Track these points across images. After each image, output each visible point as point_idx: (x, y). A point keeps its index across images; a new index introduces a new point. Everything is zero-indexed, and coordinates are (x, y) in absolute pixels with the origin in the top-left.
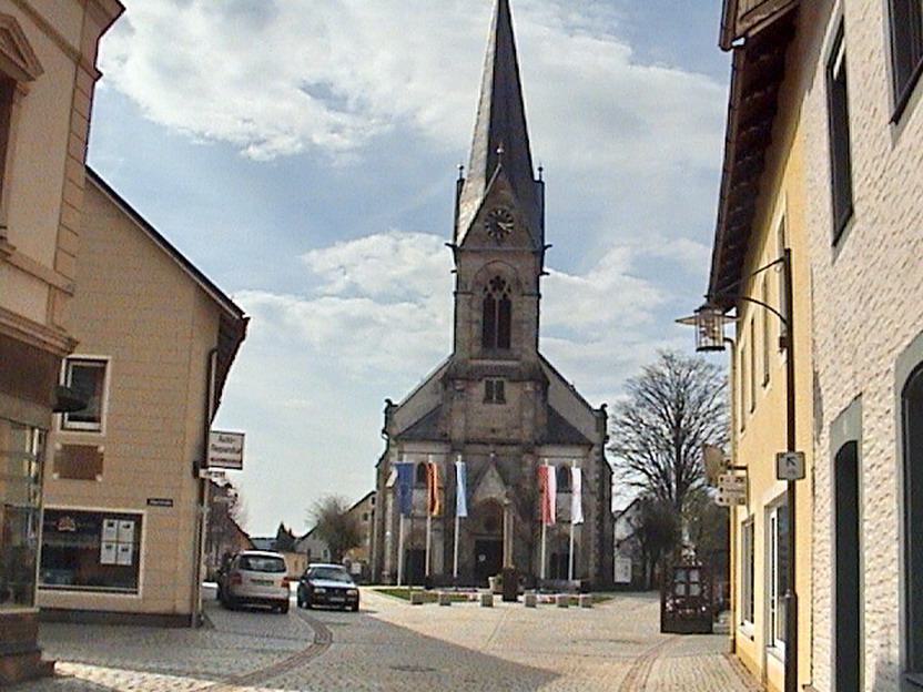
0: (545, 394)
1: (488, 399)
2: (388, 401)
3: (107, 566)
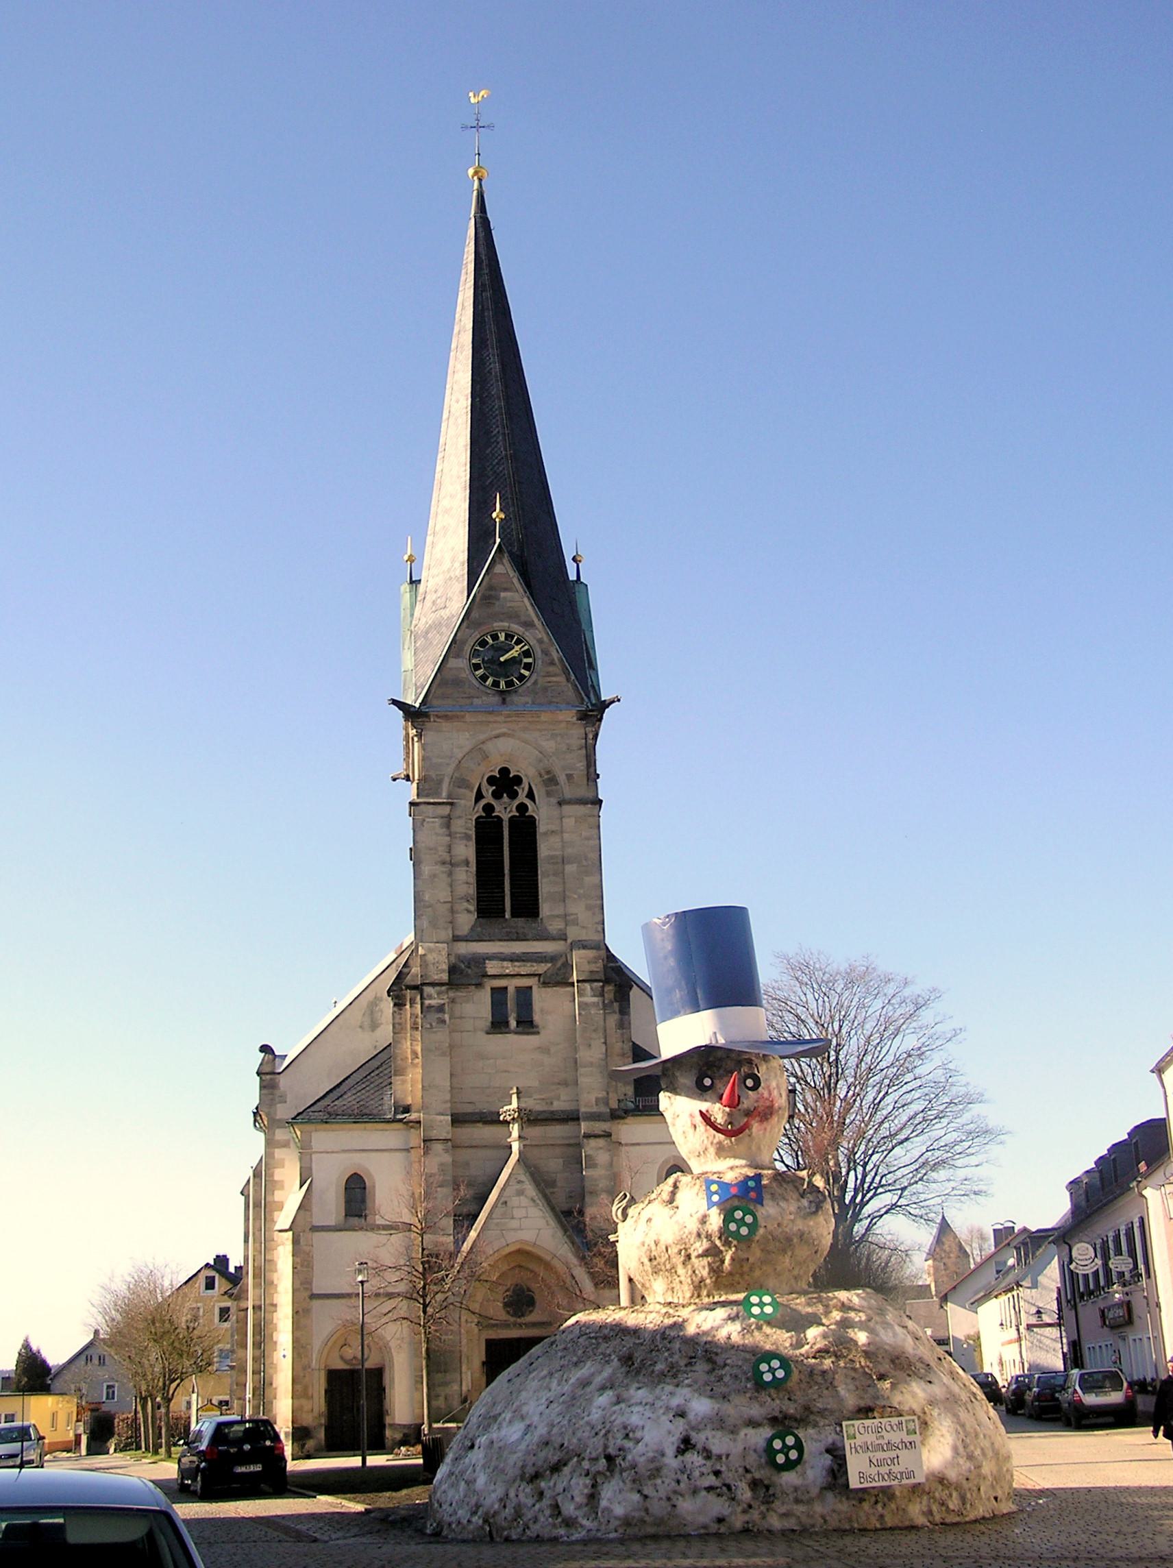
0: (624, 1010)
1: (498, 1025)
2: (265, 1049)
3: (424, 1461)
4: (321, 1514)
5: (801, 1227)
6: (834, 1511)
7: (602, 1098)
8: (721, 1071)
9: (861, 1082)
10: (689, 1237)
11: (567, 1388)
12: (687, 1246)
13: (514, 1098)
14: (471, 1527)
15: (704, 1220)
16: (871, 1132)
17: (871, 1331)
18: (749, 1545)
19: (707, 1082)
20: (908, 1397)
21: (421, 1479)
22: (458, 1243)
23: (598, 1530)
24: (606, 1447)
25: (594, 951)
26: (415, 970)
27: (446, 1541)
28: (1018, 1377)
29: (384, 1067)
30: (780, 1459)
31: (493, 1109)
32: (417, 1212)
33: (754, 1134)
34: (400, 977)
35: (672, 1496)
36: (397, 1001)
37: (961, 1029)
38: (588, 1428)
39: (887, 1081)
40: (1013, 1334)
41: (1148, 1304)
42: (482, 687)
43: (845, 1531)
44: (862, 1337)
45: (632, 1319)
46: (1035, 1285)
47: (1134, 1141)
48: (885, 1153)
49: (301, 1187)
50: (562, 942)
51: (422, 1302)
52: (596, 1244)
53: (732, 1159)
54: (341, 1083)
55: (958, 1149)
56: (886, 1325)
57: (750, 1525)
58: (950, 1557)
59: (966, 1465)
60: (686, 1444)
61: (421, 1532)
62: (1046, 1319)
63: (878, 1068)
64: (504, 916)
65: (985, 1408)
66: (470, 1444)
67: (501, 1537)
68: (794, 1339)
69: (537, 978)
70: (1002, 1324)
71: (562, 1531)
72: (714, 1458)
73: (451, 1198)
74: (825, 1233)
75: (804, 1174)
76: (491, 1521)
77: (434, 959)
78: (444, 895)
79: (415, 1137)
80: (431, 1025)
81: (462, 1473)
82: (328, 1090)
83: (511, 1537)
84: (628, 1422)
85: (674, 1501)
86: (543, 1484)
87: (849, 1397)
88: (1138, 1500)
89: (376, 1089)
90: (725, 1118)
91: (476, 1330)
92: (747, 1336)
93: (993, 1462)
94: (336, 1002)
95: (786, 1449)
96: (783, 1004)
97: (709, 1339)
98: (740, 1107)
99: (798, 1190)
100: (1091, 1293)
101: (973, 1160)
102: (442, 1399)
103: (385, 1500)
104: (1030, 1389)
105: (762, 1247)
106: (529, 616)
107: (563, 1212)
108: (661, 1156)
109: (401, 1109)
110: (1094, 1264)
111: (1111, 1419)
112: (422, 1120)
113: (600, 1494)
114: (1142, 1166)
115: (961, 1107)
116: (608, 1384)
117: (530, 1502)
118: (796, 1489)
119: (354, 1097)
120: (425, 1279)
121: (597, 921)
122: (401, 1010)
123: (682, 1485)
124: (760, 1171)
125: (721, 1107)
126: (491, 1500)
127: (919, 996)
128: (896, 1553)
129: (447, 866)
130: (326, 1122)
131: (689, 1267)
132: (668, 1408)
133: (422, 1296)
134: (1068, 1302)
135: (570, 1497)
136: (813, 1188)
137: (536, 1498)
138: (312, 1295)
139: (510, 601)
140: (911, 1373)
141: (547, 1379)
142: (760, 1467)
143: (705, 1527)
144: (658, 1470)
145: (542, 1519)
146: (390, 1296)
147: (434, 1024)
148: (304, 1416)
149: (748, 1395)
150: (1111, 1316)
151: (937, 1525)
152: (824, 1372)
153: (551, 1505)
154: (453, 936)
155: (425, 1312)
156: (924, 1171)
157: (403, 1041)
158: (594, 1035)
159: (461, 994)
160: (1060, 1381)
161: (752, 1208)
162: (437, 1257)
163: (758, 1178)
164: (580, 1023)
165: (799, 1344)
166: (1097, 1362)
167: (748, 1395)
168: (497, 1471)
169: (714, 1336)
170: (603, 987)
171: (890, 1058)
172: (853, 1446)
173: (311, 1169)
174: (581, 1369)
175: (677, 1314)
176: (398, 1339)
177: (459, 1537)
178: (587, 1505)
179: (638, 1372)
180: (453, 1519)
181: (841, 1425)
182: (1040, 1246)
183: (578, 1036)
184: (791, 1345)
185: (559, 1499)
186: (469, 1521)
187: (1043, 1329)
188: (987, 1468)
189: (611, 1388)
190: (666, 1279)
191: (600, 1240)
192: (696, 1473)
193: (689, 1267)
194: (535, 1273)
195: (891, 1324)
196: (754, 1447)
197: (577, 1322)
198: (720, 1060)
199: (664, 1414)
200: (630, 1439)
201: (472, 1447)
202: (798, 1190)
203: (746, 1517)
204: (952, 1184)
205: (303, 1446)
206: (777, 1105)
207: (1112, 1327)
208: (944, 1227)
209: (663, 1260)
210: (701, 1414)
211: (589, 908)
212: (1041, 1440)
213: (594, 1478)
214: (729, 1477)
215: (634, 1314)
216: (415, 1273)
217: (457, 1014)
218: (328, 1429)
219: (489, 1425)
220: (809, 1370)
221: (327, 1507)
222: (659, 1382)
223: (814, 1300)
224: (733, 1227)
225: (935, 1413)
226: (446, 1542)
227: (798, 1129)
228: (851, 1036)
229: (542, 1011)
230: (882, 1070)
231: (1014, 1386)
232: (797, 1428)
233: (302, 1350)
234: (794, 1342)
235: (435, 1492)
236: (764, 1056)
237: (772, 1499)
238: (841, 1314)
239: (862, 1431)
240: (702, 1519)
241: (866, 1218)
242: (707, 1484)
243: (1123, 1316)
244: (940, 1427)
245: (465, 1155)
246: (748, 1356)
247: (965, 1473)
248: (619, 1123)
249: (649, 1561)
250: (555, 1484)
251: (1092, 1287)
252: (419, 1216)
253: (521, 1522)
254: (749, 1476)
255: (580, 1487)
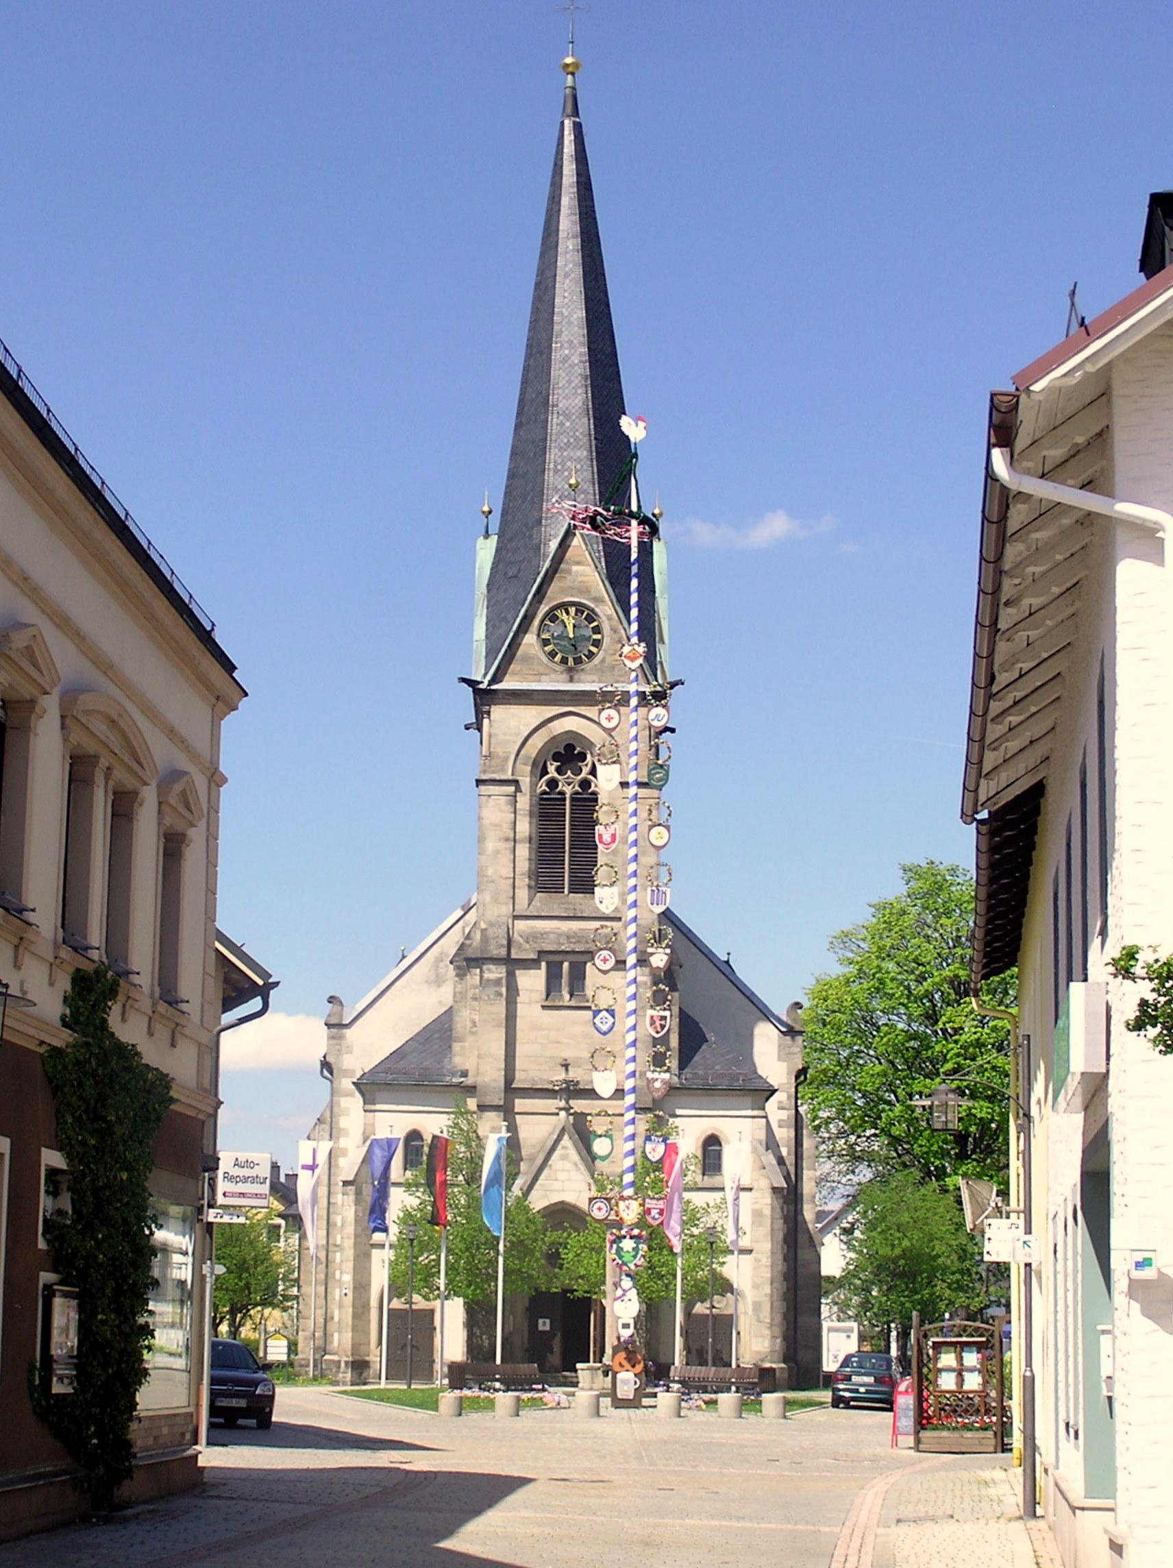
42: (550, 664)
49: (364, 1143)
106: (599, 591)
139: (582, 575)
147: (492, 997)
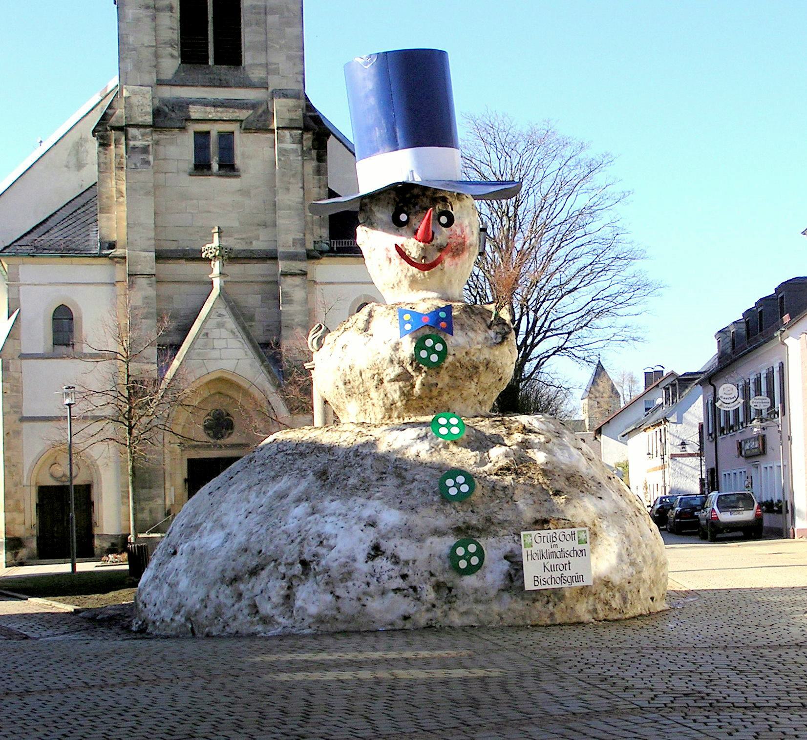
0: (321, 158)
1: (201, 167)
4: (32, 614)
5: (487, 357)
6: (509, 610)
7: (299, 240)
8: (417, 208)
9: (537, 235)
10: (382, 363)
11: (264, 500)
12: (380, 371)
13: (216, 236)
14: (174, 625)
15: (396, 348)
16: (543, 281)
17: (549, 452)
18: (433, 639)
19: (403, 217)
20: (580, 511)
21: (127, 582)
22: (162, 371)
23: (293, 627)
24: (301, 553)
25: (294, 100)
26: (120, 111)
27: (150, 636)
28: (662, 498)
29: (91, 204)
30: (463, 564)
31: (196, 247)
32: (122, 342)
33: (445, 269)
34: (105, 118)
35: (362, 597)
36: (102, 141)
37: (629, 192)
38: (285, 536)
39: (559, 236)
40: (658, 462)
41: (781, 437)
43: (518, 626)
44: (540, 457)
45: (326, 438)
46: (680, 421)
47: (780, 295)
48: (555, 300)
50: (264, 90)
51: (127, 424)
52: (291, 374)
53: (425, 292)
54: (47, 220)
55: (620, 299)
56: (563, 446)
57: (433, 622)
58: (615, 648)
59: (629, 570)
60: (376, 551)
61: (127, 629)
62: (689, 450)
63: (552, 223)
64: (207, 63)
65: (647, 522)
66: (172, 551)
67: (202, 634)
68: (478, 457)
69: (238, 124)
70: (649, 454)
71: (259, 628)
72: (401, 563)
73: (155, 329)
74: (509, 363)
75: (492, 307)
76: (193, 619)
77: (139, 101)
78: (148, 39)
79: (121, 272)
80: (135, 164)
81: (166, 576)
82: (34, 225)
83: (212, 633)
84: (322, 531)
85: (364, 602)
86: (242, 587)
87: (527, 510)
88: (771, 599)
89: (83, 225)
90: (419, 252)
91: (179, 451)
92: (434, 455)
93: (652, 568)
94: (41, 142)
95: (468, 556)
96: (469, 162)
97: (399, 456)
98: (434, 242)
99: (485, 321)
100: (732, 428)
101: (633, 310)
102: (147, 512)
103: (94, 601)
104: (673, 508)
105: (450, 373)
107: (260, 344)
108: (356, 293)
109: (107, 245)
110: (736, 402)
111: (740, 534)
112: (127, 255)
113: (294, 595)
114: (786, 318)
115: (626, 261)
116: (304, 496)
117: (229, 602)
118: (476, 590)
119: (61, 232)
120: (130, 403)
121: (297, 71)
122: (106, 150)
123: (372, 587)
124: (450, 303)
125: (416, 242)
126: (193, 601)
127: (593, 160)
128: (568, 645)
129: (151, 10)
130: (33, 256)
131: (382, 390)
132: (360, 519)
133: (128, 419)
134: (710, 435)
135: (267, 598)
136: (501, 322)
137: (235, 599)
138: (23, 417)
140: (584, 490)
141: (246, 492)
142: (444, 571)
143: (392, 624)
144: (350, 573)
145: (241, 617)
146: (97, 419)
148: (17, 527)
149: (435, 507)
150: (747, 447)
151: (600, 621)
152: (505, 488)
153: (249, 605)
154: (158, 80)
155: (130, 433)
156: (589, 318)
157: (109, 180)
158: (292, 180)
159: (165, 137)
160: (698, 502)
161: (442, 337)
162: (142, 383)
163: (448, 309)
164: (279, 168)
165: (483, 463)
166: (730, 486)
167: (435, 507)
168: (198, 576)
169: (404, 454)
170: (302, 134)
171: (563, 216)
172: (529, 553)
173: (18, 300)
174: (278, 483)
175: (369, 433)
176: (105, 458)
177: (163, 633)
178: (283, 604)
179: (332, 485)
180: (158, 617)
181: (519, 535)
182: (687, 387)
183: (277, 181)
184: (475, 463)
185: (257, 599)
186: (172, 619)
187: (684, 459)
188: (647, 573)
189: (307, 500)
190: (359, 402)
191: (296, 370)
192: (385, 577)
193: (382, 390)
194: (235, 400)
195: (566, 446)
196: (438, 554)
197: (275, 439)
198: (417, 196)
199: (356, 524)
200: (324, 547)
201: (175, 553)
202: (485, 321)
203: (430, 615)
204: (614, 330)
205: (16, 554)
206: (468, 242)
207: (747, 457)
208: (600, 370)
209: (357, 383)
210: (391, 524)
211: (289, 58)
212: (683, 550)
213: (290, 581)
214: (415, 580)
215: (329, 433)
216: (122, 398)
217: (161, 156)
218: (39, 539)
219: (191, 534)
220: (491, 485)
221: (38, 608)
222: (352, 495)
223: (498, 423)
224: (424, 354)
225: (604, 525)
226: (150, 639)
227: (477, 276)
228: (530, 193)
229: (243, 155)
230: (556, 226)
231: (659, 506)
232: (479, 537)
233: (14, 468)
234: (478, 460)
235: (140, 594)
236: (459, 194)
237: (454, 599)
238: (522, 436)
239: (538, 540)
240: (389, 617)
241: (536, 358)
242: (394, 586)
243: (758, 448)
244: (608, 538)
245: (167, 289)
246: (435, 472)
247: (627, 577)
248: (313, 263)
249: (341, 654)
250: (253, 587)
251: (731, 423)
252: (125, 344)
253: (222, 620)
254: (433, 579)
255: (277, 589)
